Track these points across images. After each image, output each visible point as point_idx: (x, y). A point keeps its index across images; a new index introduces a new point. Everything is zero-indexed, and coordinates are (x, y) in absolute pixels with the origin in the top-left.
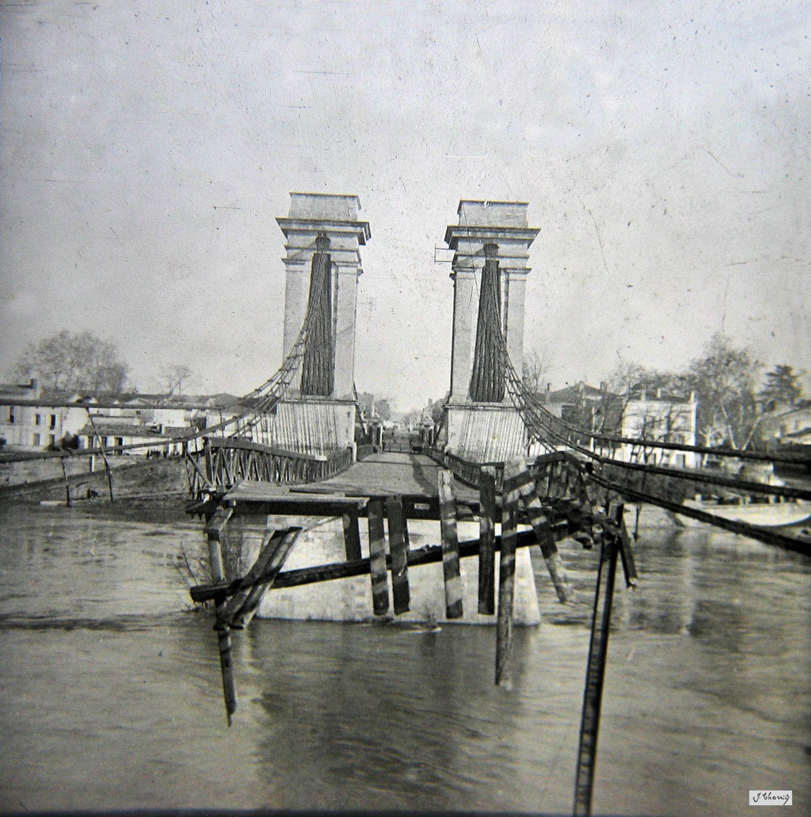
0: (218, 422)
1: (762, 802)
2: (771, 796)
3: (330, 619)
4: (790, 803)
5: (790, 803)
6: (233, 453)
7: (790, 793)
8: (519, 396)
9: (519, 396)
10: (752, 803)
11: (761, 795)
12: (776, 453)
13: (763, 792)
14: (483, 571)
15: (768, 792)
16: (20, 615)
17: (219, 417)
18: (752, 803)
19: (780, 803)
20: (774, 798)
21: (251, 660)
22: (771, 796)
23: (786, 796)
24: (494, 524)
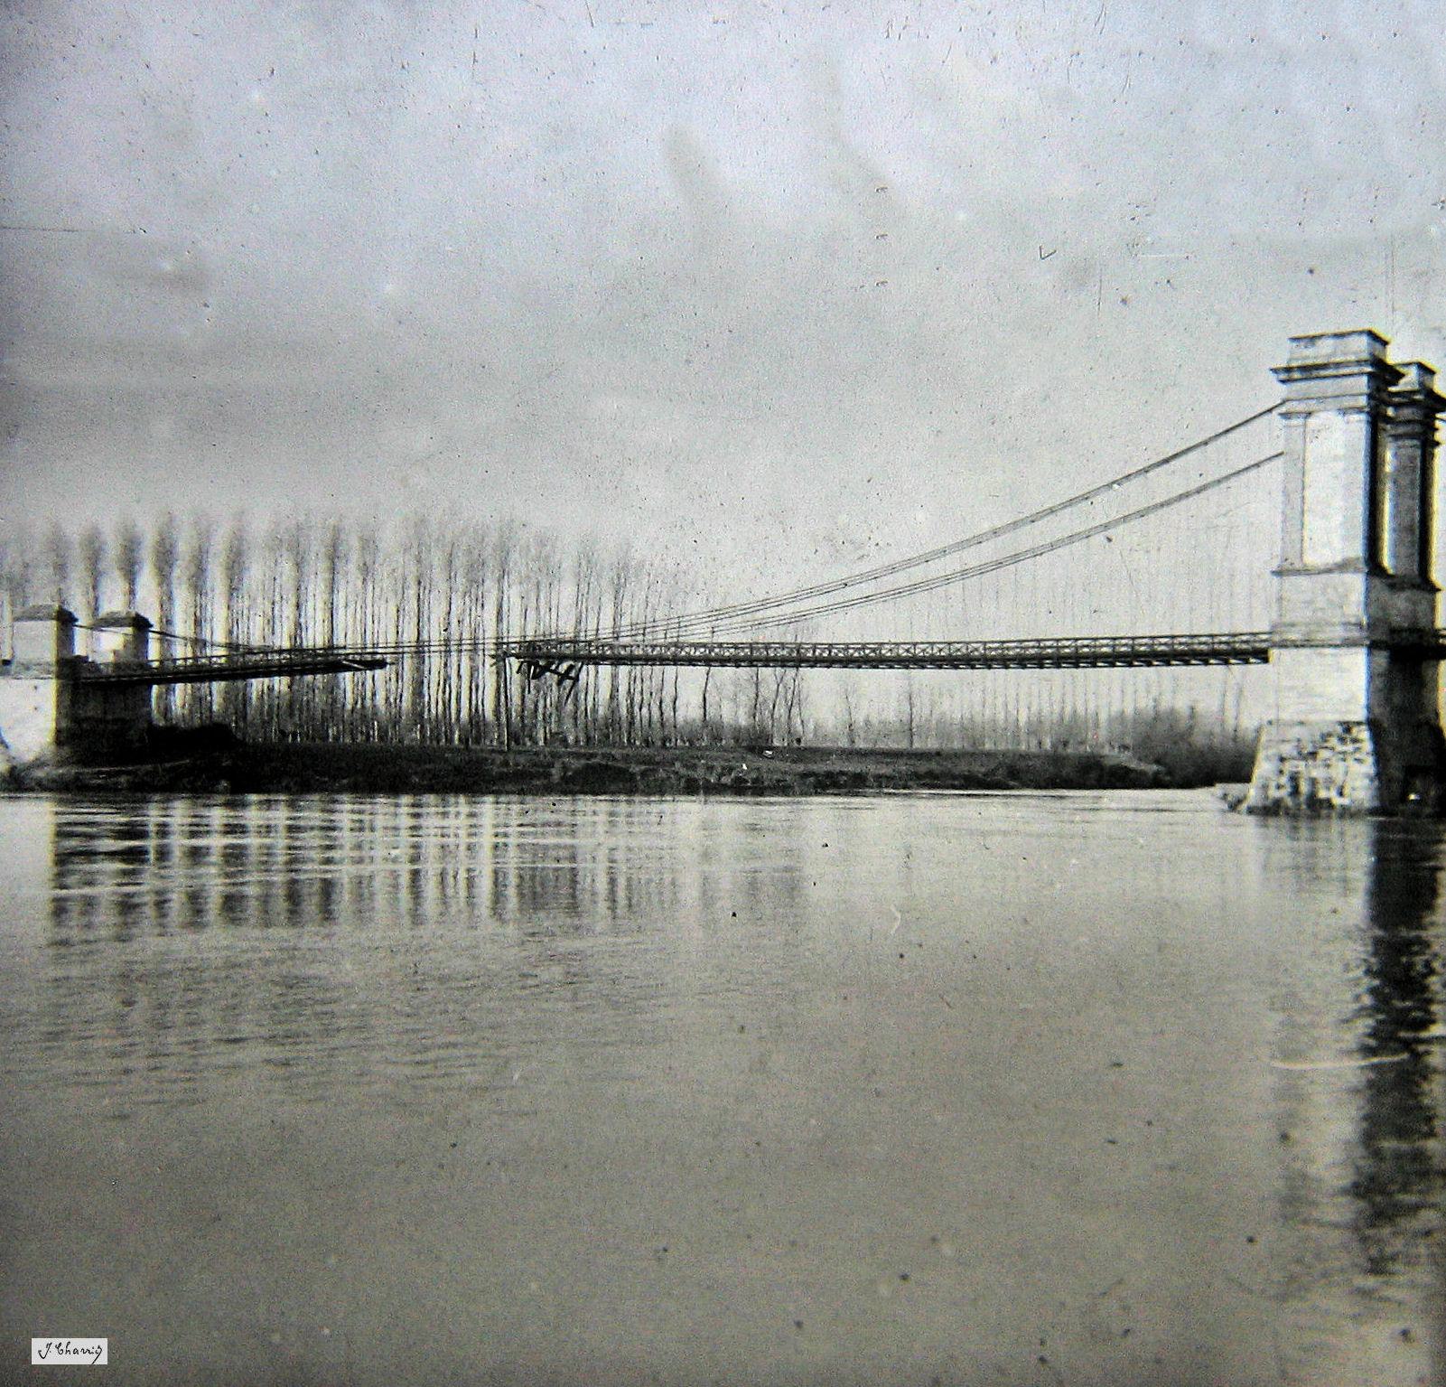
1: (54, 1359)
2: (71, 1348)
4: (103, 1360)
5: (103, 1360)
7: (104, 1342)
10: (36, 1360)
11: (53, 1347)
13: (56, 1341)
15: (64, 1341)
20: (76, 1352)
21: (493, 653)
22: (71, 1348)
23: (96, 1348)
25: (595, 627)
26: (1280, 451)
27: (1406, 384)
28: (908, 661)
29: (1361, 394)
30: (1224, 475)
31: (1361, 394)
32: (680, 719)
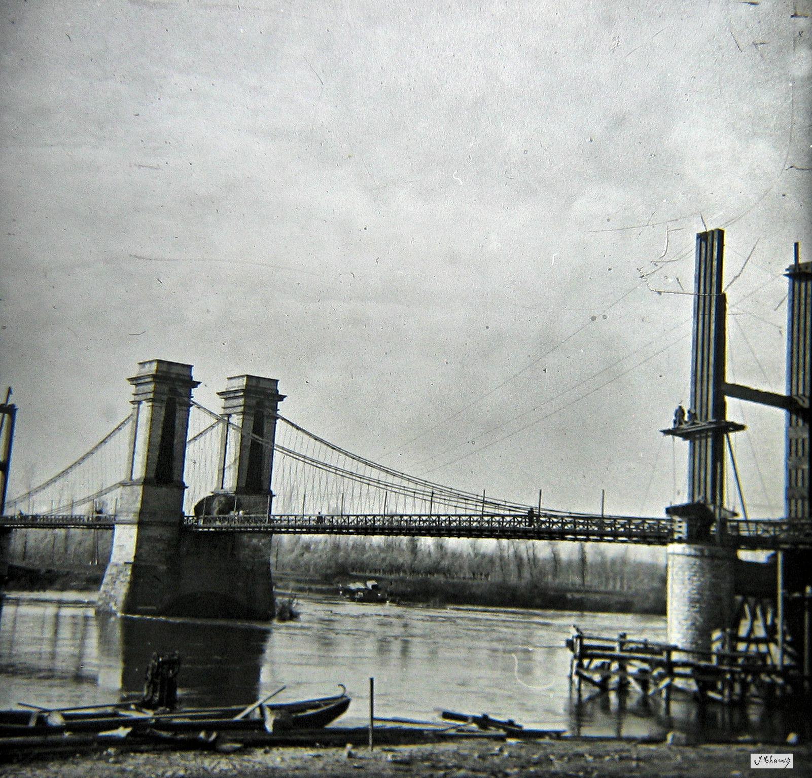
0: (751, 529)
1: (763, 765)
2: (773, 759)
3: (88, 635)
4: (791, 766)
5: (791, 766)
6: (364, 580)
7: (791, 756)
8: (281, 517)
9: (281, 517)
10: (753, 766)
11: (762, 758)
12: (570, 586)
13: (764, 755)
14: (270, 468)
15: (769, 755)
16: (297, 530)
17: (6, 574)
18: (753, 766)
19: (781, 766)
20: (775, 761)
21: (590, 558)
22: (773, 759)
23: (787, 759)
24: (738, 651)
25: (453, 508)
26: (369, 681)
27: (340, 722)
28: (160, 740)
29: (706, 229)
30: (308, 667)
31: (706, 229)
32: (687, 646)
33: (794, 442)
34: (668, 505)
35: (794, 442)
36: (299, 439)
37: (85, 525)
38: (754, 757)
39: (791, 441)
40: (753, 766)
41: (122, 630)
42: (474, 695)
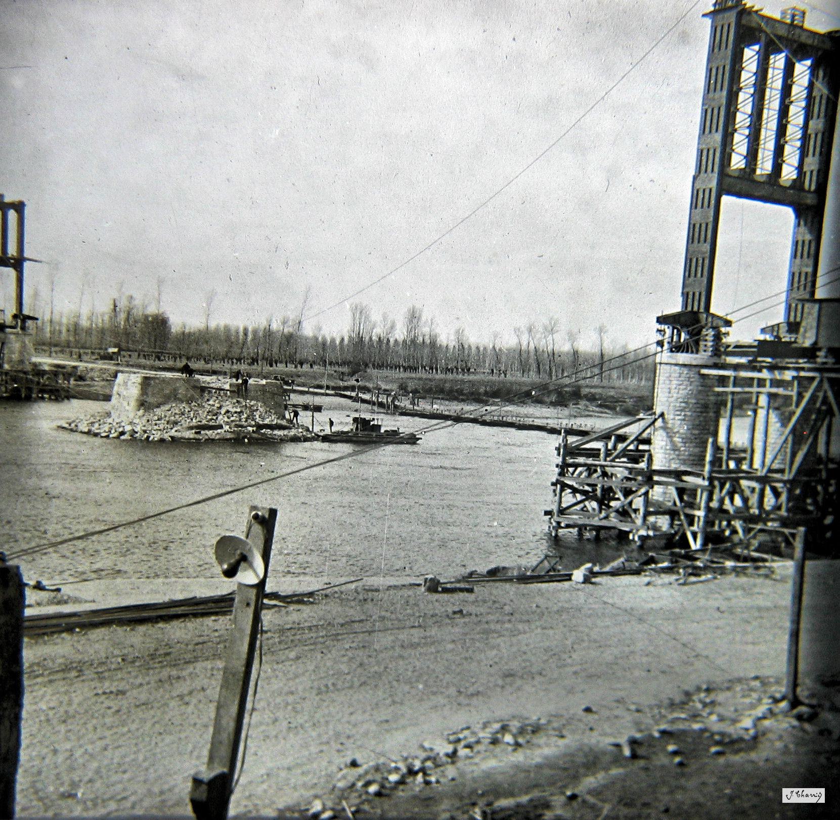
1: (795, 800)
2: (804, 793)
4: (822, 800)
5: (822, 800)
7: (823, 790)
9: (812, 299)
10: (785, 800)
13: (796, 790)
15: (801, 790)
19: (813, 800)
20: (807, 796)
22: (804, 793)
33: (800, 244)
34: (660, 315)
35: (800, 244)
36: (775, 301)
37: (344, 363)
38: (786, 791)
39: (794, 274)
40: (785, 800)
41: (21, 657)
42: (810, 270)
